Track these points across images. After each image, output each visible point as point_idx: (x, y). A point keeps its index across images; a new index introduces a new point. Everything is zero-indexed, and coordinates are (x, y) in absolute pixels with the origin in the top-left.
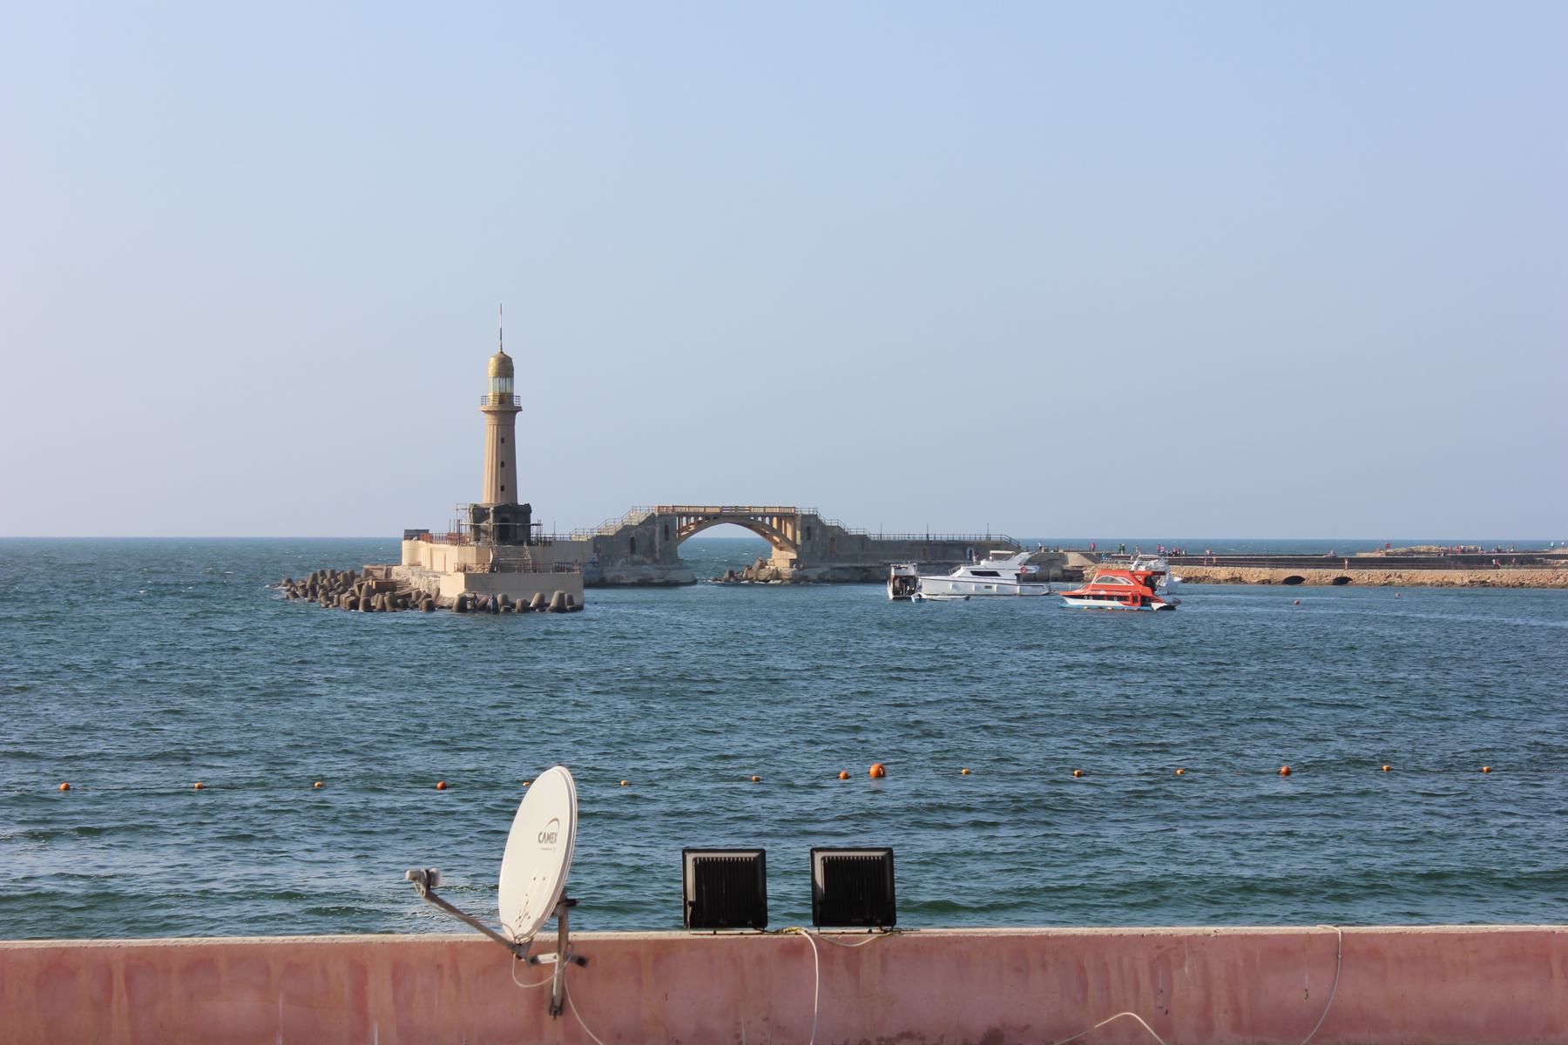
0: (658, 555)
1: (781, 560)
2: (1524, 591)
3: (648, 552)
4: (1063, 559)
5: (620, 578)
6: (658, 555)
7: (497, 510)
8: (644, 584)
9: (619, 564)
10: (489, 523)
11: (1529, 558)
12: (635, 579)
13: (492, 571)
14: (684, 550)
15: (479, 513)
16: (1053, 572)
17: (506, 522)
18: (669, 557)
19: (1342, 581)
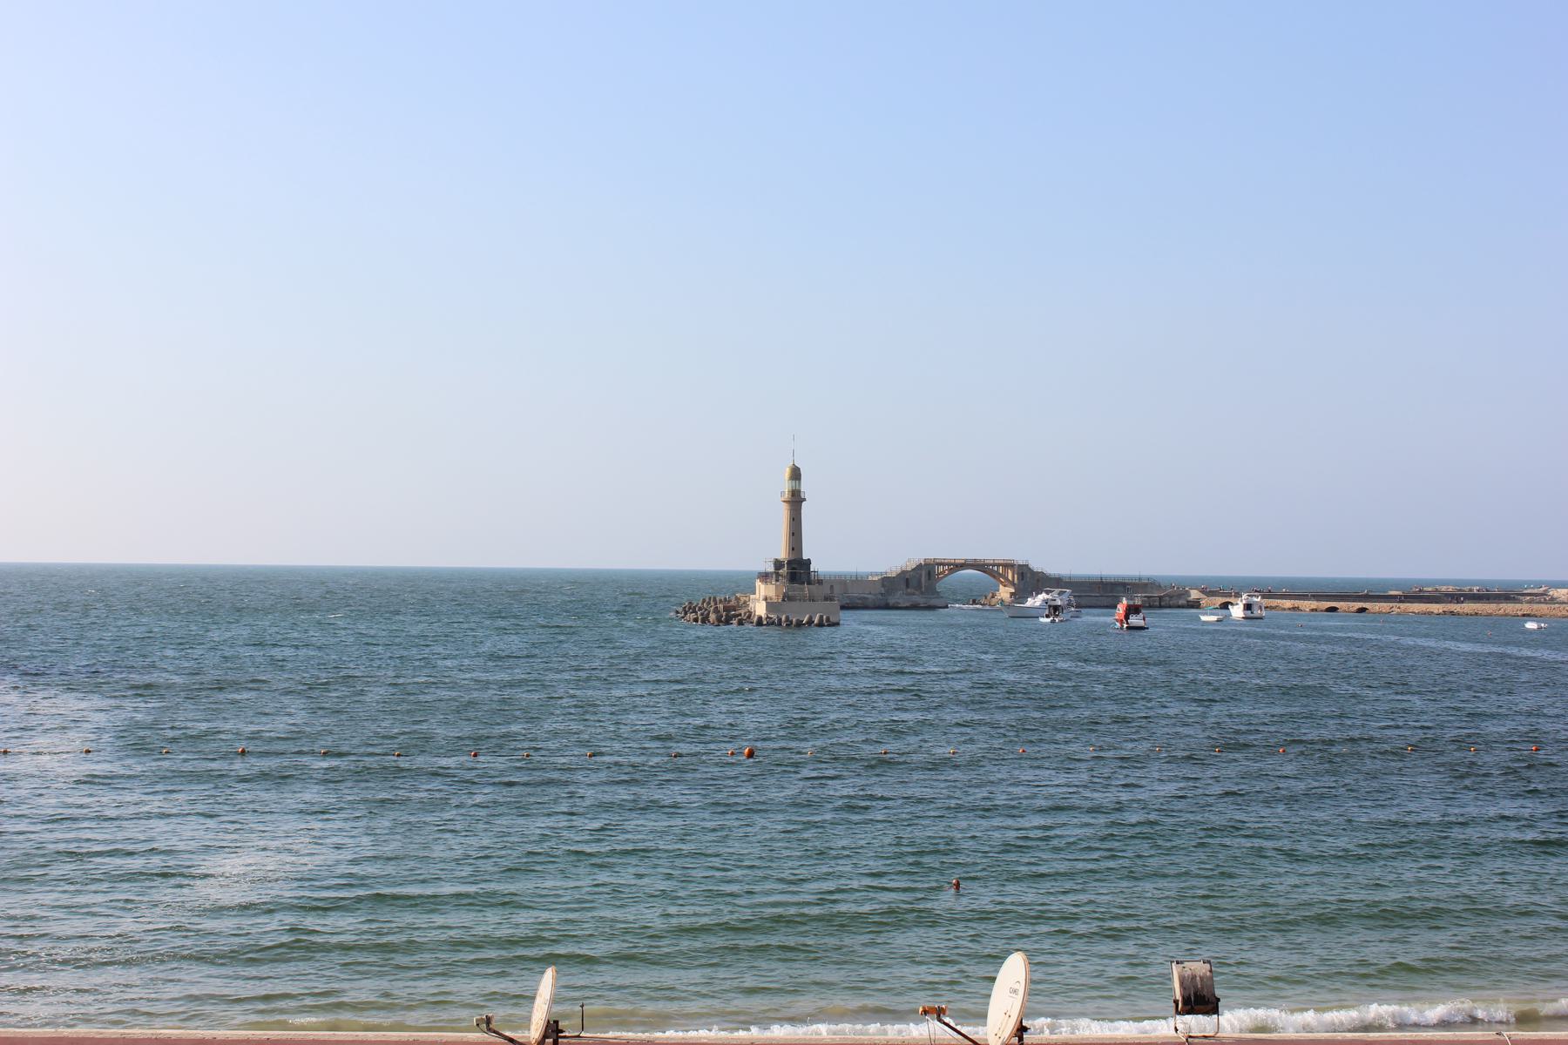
1: (1005, 593)
2: (1454, 619)
3: (917, 588)
8: (915, 607)
10: (784, 571)
11: (1507, 597)
14: (940, 586)
15: (778, 564)
16: (1181, 602)
17: (796, 570)
18: (931, 590)
19: (1362, 610)
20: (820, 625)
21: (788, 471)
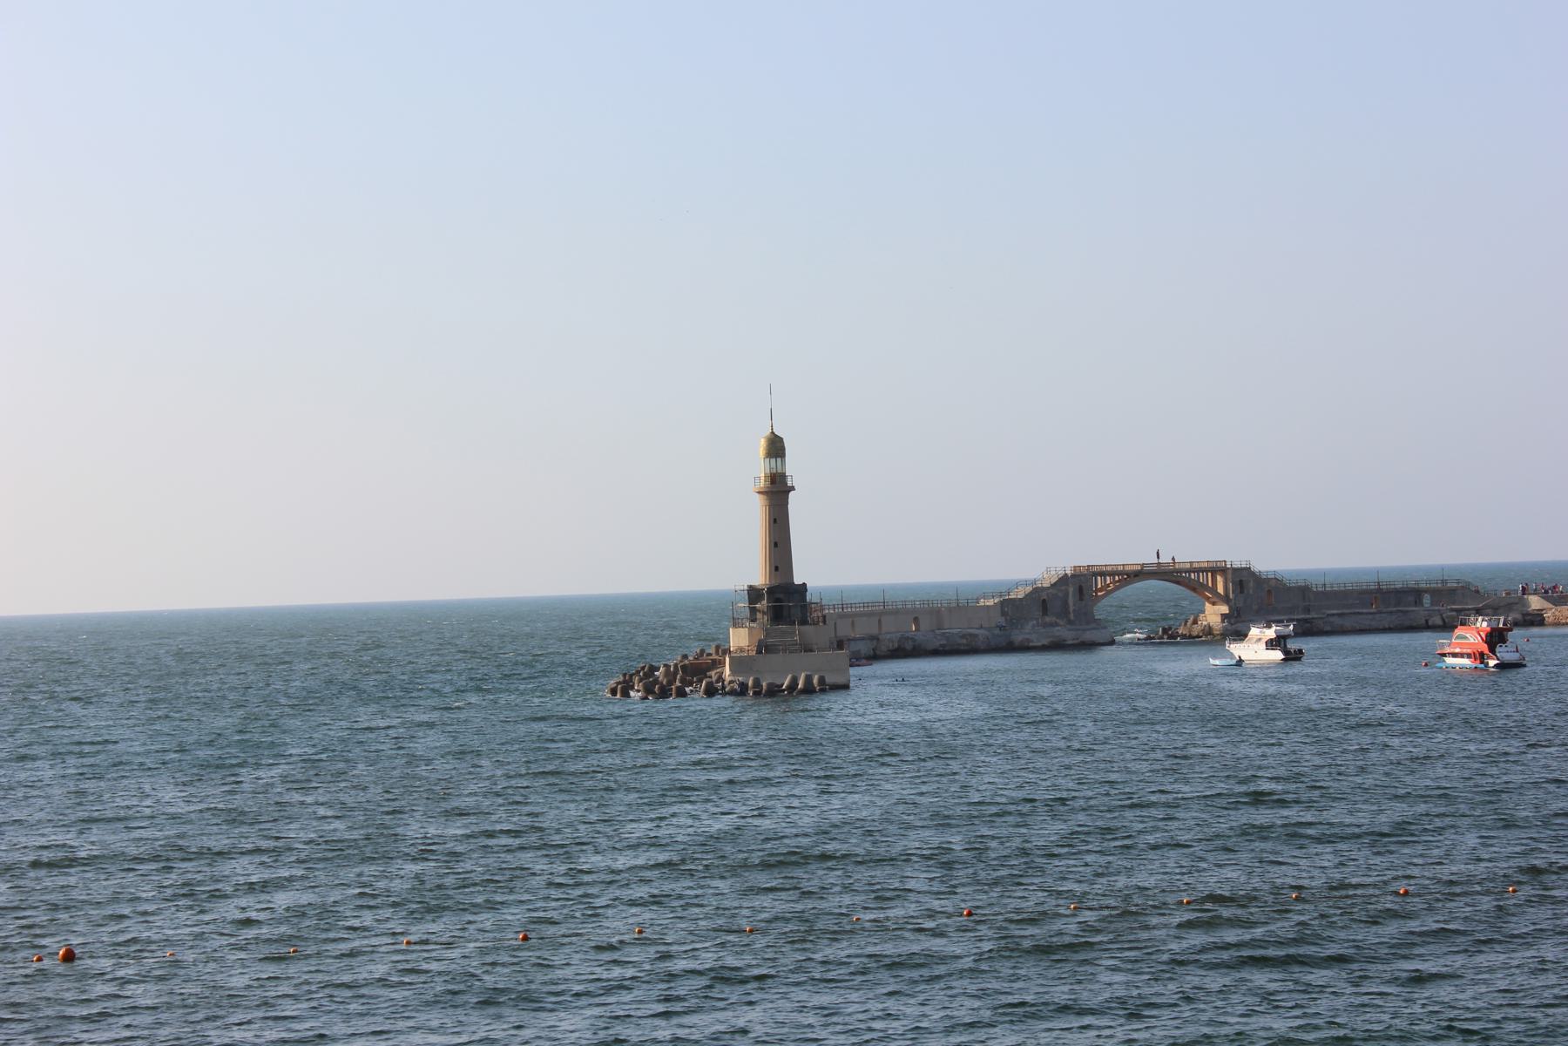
0: (1072, 617)
4: (1522, 602)
5: (1028, 640)
6: (1072, 617)
7: (771, 590)
8: (1058, 646)
9: (1028, 627)
10: (763, 604)
12: (1045, 642)
13: (759, 652)
14: (1102, 610)
17: (782, 601)
20: (809, 690)
21: (763, 443)
